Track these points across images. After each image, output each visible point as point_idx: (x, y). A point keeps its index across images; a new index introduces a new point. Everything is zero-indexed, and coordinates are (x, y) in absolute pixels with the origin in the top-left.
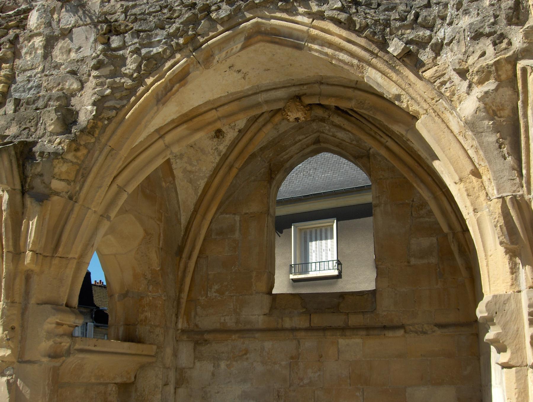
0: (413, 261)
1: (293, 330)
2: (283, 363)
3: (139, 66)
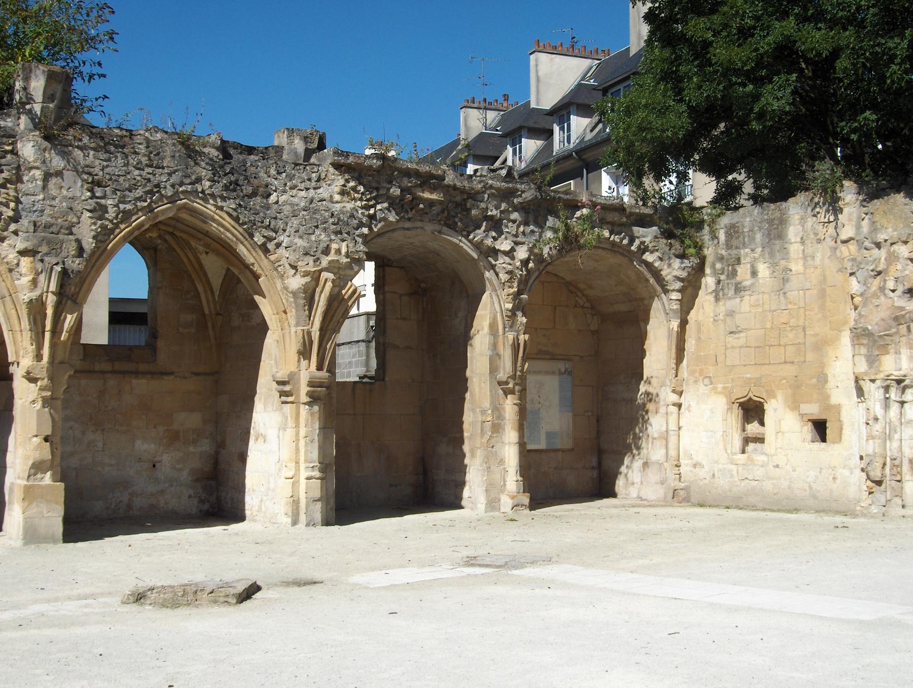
0: (181, 330)
1: (103, 372)
2: (94, 395)
3: (117, 215)
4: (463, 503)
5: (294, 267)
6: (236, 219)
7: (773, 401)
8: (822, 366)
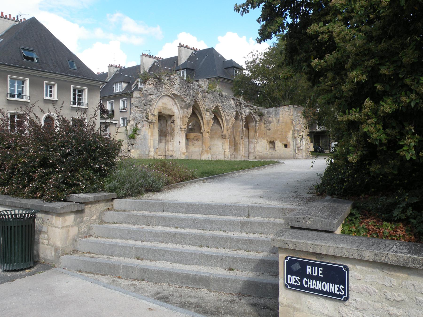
7: (277, 141)
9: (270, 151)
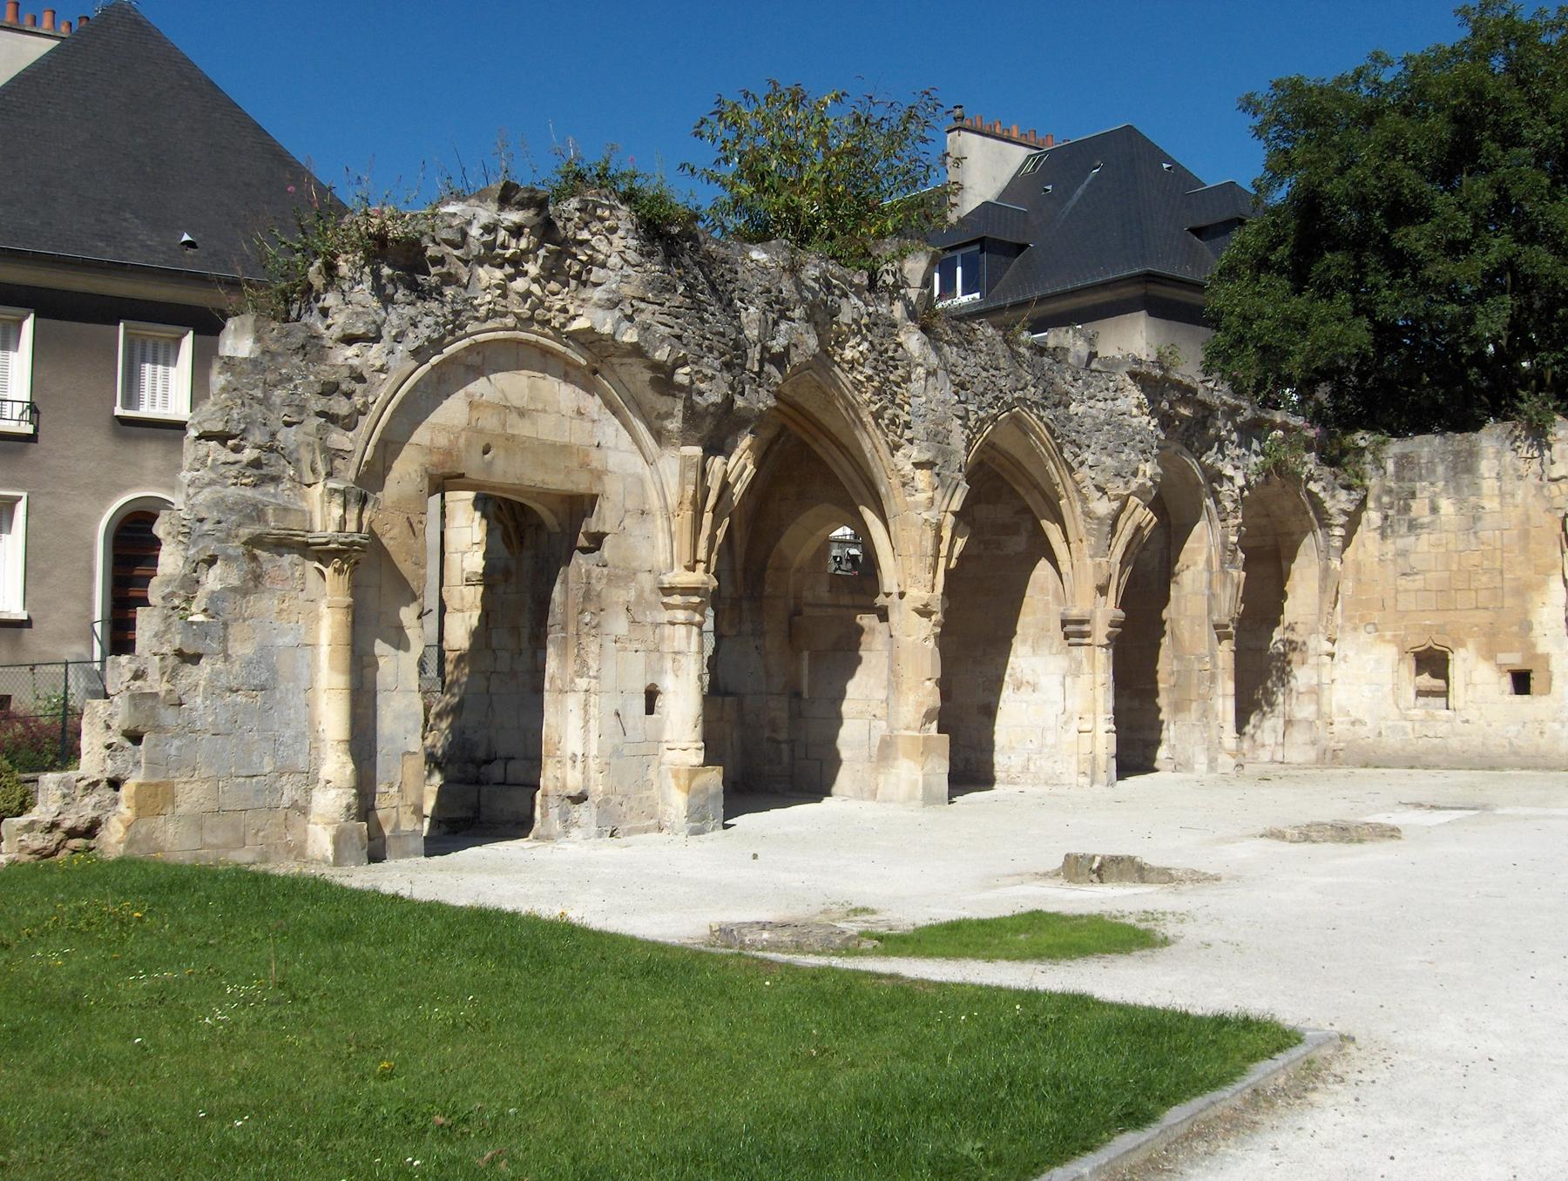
4: (1157, 765)
5: (1099, 488)
6: (1051, 432)
7: (1462, 650)
8: (1526, 612)
9: (1418, 713)
